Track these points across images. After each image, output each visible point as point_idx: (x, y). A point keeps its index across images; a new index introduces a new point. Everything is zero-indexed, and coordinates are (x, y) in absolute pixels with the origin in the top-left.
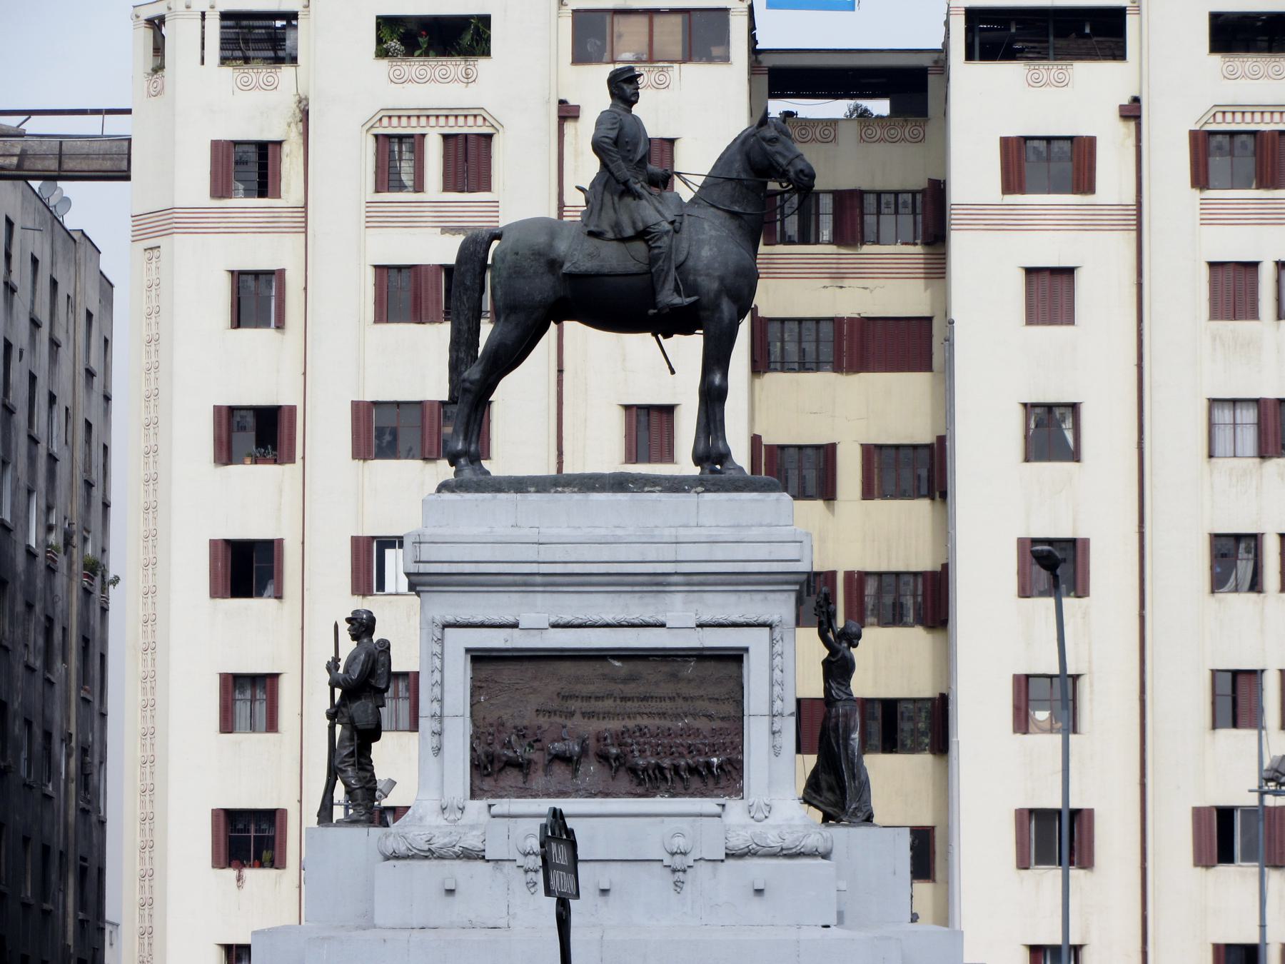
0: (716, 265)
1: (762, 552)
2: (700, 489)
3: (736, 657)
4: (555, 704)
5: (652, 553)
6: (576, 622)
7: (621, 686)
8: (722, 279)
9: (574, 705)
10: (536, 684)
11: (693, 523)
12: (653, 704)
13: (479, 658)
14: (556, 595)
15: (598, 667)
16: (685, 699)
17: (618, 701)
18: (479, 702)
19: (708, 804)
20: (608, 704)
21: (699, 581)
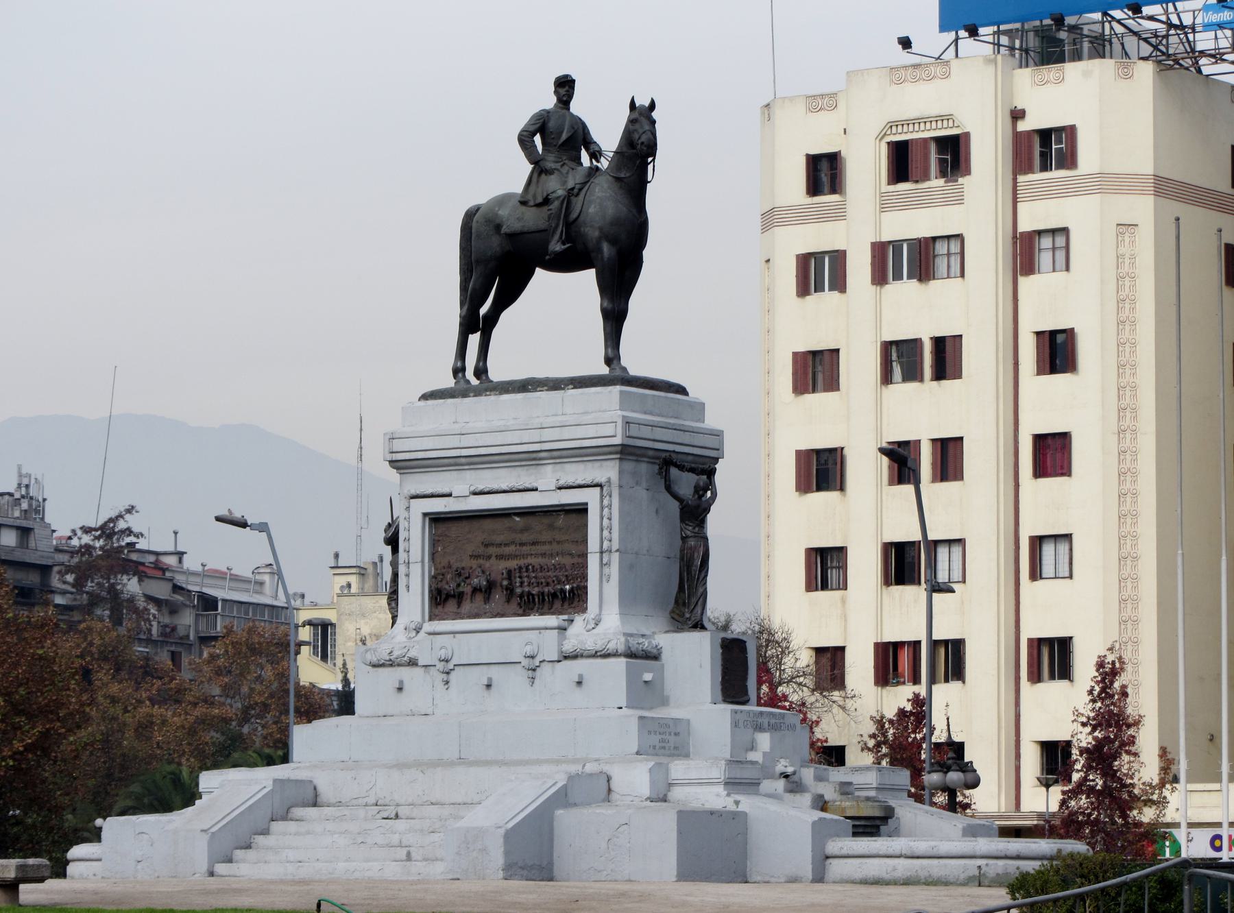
1: (591, 431)
3: (581, 510)
4: (481, 550)
5: (527, 436)
9: (492, 550)
13: (436, 519)
15: (506, 522)
16: (558, 542)
19: (552, 620)
21: (561, 455)
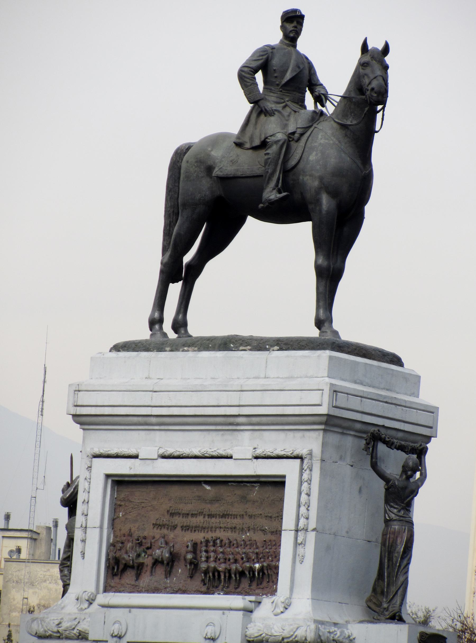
0: (318, 167)
1: (295, 398)
2: (276, 348)
3: (278, 483)
4: (166, 519)
5: (224, 399)
6: (176, 454)
7: (209, 506)
8: (321, 179)
9: (178, 520)
10: (155, 503)
11: (263, 376)
12: (229, 520)
13: (119, 482)
14: (169, 433)
16: (250, 517)
17: (207, 517)
18: (118, 517)
20: (199, 520)
